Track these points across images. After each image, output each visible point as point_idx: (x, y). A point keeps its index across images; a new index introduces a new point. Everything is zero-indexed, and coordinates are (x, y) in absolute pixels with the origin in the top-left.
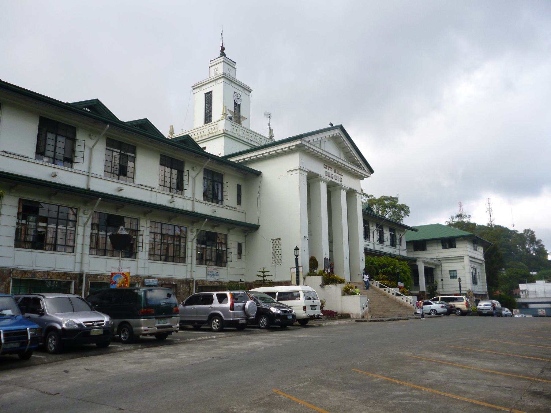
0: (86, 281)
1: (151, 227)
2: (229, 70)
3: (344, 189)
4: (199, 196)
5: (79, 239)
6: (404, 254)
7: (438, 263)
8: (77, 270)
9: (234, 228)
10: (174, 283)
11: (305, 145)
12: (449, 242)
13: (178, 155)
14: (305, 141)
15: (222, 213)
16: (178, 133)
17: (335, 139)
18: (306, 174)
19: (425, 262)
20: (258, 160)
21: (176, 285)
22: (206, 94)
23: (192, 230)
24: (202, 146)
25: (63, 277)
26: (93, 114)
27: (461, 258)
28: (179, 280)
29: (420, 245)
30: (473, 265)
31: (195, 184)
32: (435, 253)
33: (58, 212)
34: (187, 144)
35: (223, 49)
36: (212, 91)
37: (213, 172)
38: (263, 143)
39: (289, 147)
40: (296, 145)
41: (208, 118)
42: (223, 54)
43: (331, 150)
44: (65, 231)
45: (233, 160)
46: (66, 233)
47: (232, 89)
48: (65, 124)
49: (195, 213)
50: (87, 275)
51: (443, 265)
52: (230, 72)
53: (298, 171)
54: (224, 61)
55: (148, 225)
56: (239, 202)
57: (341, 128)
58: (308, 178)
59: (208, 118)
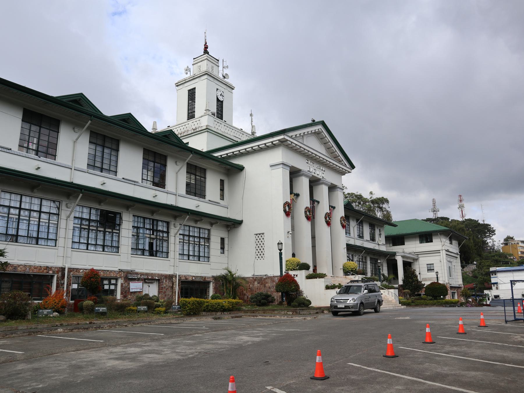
0: (68, 275)
1: (134, 221)
2: (213, 67)
3: (326, 184)
4: (183, 190)
5: (62, 233)
6: (383, 248)
7: (415, 257)
8: (60, 264)
9: (217, 223)
10: (157, 278)
11: (287, 140)
12: (426, 237)
13: (161, 149)
14: (288, 136)
15: (204, 207)
16: (161, 128)
17: (317, 134)
18: (289, 169)
19: (403, 257)
20: (241, 155)
21: (159, 280)
22: (189, 91)
23: (174, 224)
24: (185, 141)
25: (45, 271)
26: (76, 109)
27: (438, 252)
28: (162, 275)
29: (398, 240)
30: (449, 259)
31: (177, 176)
32: (412, 247)
33: (505, 316)
34: (168, 138)
35: (206, 47)
36: (195, 88)
37: (196, 166)
38: (244, 138)
39: (272, 142)
40: (279, 140)
41: (191, 115)
42: (206, 52)
43: (313, 145)
44: (47, 224)
45: (216, 155)
46: (49, 226)
47: (215, 85)
48: (47, 114)
49: (178, 207)
50: (69, 269)
51: (421, 259)
52: (213, 70)
53: (281, 166)
54: (207, 59)
55: (131, 218)
56: (222, 197)
57: (323, 123)
58: (291, 173)
59: (191, 115)
